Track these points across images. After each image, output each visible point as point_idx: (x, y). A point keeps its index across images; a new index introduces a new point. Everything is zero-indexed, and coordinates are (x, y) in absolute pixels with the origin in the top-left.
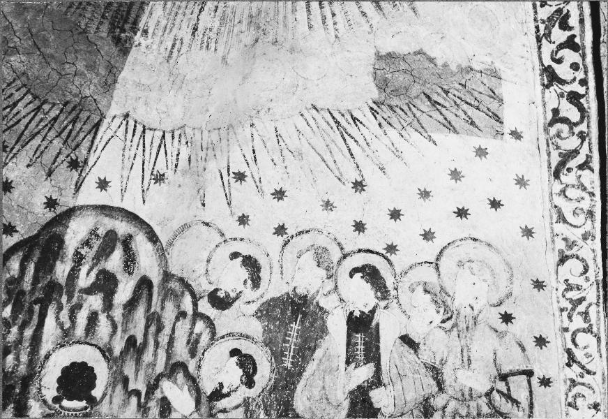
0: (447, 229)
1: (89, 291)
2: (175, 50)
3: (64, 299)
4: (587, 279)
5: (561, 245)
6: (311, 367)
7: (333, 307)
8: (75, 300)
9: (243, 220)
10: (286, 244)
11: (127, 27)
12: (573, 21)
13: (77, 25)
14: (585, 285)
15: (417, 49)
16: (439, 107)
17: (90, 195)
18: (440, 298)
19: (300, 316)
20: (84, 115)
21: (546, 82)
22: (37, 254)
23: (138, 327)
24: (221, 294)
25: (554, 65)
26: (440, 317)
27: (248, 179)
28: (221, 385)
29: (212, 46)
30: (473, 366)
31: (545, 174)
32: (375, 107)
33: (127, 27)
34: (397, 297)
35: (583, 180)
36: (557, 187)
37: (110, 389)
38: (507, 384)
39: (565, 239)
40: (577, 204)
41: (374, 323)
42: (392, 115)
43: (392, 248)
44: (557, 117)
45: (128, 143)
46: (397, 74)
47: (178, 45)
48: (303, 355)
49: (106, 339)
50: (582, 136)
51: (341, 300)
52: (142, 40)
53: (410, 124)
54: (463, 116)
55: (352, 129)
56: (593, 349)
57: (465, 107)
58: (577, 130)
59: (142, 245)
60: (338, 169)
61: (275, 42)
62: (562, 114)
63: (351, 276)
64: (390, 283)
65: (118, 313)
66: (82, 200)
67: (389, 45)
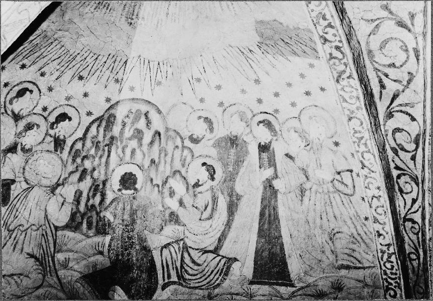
0: (302, 102)
1: (130, 139)
2: (159, 25)
3: (119, 143)
4: (363, 128)
5: (347, 112)
6: (242, 170)
7: (250, 140)
8: (124, 144)
9: (202, 100)
10: (225, 110)
11: (134, 17)
12: (328, 16)
13: (110, 20)
14: (363, 131)
15: (274, 19)
16: (289, 45)
17: (126, 94)
18: (302, 134)
19: (235, 146)
20: (118, 59)
21: (323, 42)
22: (104, 124)
23: (155, 153)
24: (195, 137)
25: (325, 35)
26: (304, 144)
27: (203, 81)
28: (199, 181)
29: (177, 20)
30: (322, 168)
31: (333, 82)
32: (259, 45)
33: (134, 17)
34: (281, 135)
35: (350, 83)
36: (339, 87)
37: (144, 184)
38: (341, 176)
39: (349, 110)
40: (350, 94)
41: (271, 148)
42: (268, 48)
43: (277, 111)
44: (332, 57)
45: (142, 68)
46: (267, 30)
47: (160, 22)
48: (238, 165)
49: (141, 161)
50: (346, 65)
51: (254, 137)
52: (142, 22)
53: (277, 52)
54: (301, 49)
55: (250, 55)
56: (372, 160)
57: (300, 45)
58: (342, 62)
59: (153, 115)
60: (246, 74)
61: (207, 17)
62: (334, 55)
63: (258, 125)
64: (277, 128)
65: (145, 148)
66: (122, 96)
67: (261, 17)
